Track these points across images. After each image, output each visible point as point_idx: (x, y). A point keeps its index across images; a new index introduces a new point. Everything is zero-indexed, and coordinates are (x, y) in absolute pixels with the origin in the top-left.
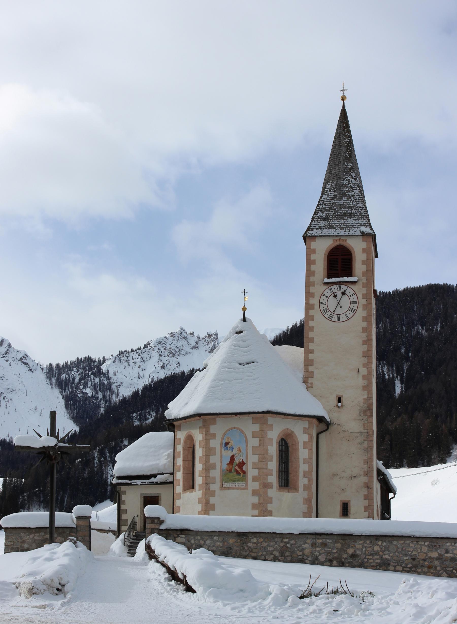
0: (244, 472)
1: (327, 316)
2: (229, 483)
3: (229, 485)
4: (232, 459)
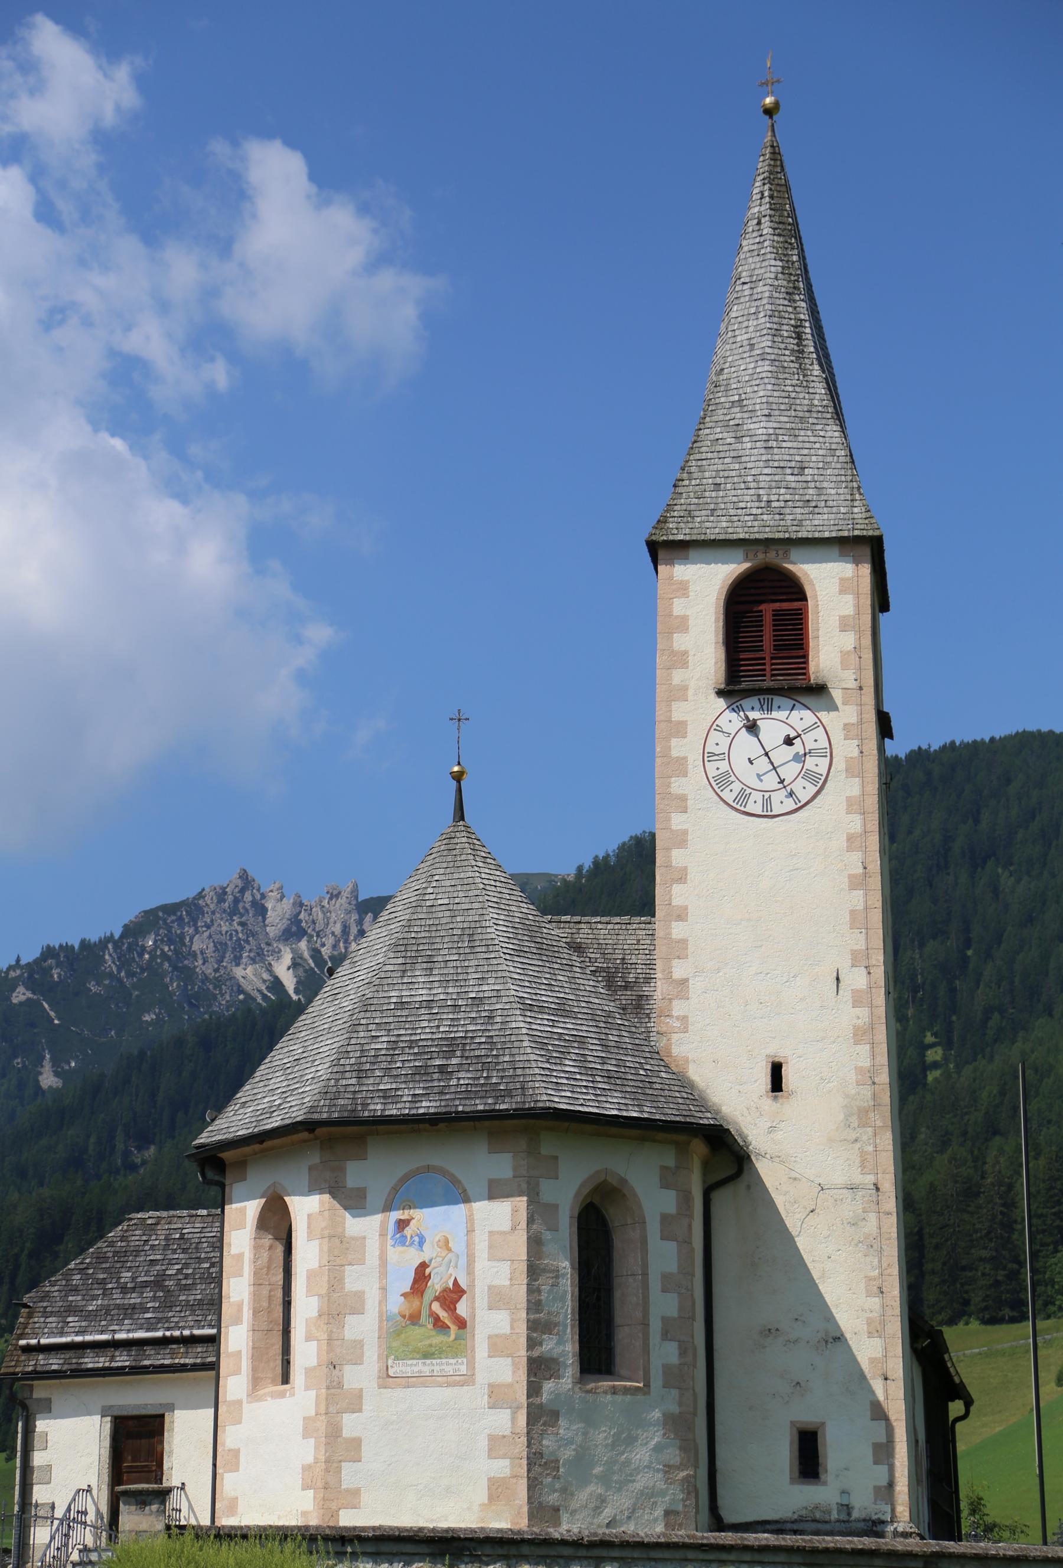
0: (462, 1324)
2: (410, 1362)
3: (409, 1369)
4: (421, 1275)
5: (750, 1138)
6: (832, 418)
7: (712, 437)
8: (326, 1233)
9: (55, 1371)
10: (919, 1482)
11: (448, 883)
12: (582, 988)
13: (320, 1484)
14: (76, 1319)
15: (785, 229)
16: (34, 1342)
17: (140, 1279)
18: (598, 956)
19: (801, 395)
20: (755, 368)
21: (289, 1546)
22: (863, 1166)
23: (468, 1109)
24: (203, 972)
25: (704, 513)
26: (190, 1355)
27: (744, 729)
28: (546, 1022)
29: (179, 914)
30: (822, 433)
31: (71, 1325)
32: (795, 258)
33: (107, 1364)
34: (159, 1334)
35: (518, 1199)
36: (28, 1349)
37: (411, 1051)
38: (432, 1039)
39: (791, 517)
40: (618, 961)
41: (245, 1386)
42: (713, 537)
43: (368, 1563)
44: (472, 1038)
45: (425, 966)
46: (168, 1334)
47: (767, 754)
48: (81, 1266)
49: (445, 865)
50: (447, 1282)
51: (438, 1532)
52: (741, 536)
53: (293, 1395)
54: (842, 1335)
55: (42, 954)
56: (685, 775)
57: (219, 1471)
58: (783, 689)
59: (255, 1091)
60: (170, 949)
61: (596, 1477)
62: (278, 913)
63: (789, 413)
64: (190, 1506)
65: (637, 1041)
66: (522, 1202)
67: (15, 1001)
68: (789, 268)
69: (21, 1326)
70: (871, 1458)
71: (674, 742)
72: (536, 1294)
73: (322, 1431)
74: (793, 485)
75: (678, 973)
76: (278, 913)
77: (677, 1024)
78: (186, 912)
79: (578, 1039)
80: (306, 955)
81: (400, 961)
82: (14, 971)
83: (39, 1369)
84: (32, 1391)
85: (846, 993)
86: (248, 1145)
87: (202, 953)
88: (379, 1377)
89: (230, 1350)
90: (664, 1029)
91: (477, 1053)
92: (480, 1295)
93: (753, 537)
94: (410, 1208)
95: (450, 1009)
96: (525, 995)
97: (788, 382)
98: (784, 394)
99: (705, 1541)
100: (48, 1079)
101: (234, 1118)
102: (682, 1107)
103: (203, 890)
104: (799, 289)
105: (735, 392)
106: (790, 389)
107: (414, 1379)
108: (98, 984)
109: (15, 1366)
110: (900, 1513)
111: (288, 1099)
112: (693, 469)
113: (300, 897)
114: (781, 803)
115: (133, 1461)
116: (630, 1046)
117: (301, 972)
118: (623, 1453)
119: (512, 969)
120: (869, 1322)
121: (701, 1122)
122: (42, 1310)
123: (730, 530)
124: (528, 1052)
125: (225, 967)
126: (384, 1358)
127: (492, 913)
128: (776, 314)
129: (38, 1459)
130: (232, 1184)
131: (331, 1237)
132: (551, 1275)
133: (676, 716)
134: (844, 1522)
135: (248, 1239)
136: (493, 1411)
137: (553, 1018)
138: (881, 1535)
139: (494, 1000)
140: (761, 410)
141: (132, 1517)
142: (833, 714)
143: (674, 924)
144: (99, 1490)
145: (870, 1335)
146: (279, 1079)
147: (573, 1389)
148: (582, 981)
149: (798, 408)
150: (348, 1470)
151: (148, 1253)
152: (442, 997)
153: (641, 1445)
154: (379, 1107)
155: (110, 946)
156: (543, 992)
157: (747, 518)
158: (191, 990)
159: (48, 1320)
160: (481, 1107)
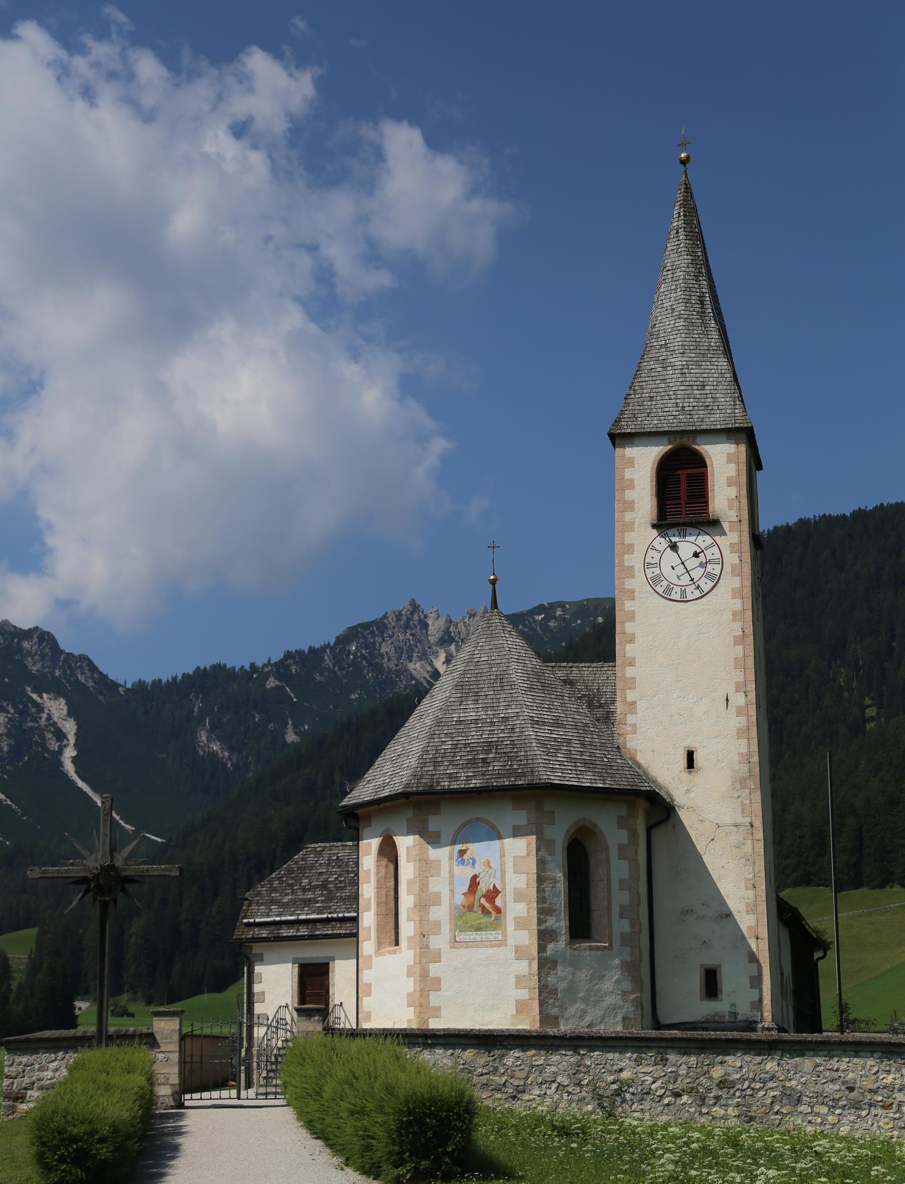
0: (498, 911)
1: (660, 589)
2: (468, 933)
3: (468, 937)
4: (474, 883)
5: (674, 797)
7: (648, 367)
8: (417, 858)
9: (264, 938)
10: (784, 997)
11: (487, 648)
12: (569, 709)
13: (417, 1004)
14: (276, 907)
15: (693, 236)
16: (252, 920)
17: (313, 884)
18: (583, 687)
19: (703, 340)
20: (675, 323)
21: (389, 1040)
22: (743, 812)
23: (499, 784)
24: (388, 666)
25: (643, 415)
26: (343, 929)
28: (547, 731)
29: (371, 629)
30: (716, 363)
32: (700, 254)
33: (294, 934)
34: (325, 916)
35: (531, 837)
36: (248, 925)
38: (478, 743)
39: (697, 416)
40: (595, 691)
41: (374, 947)
42: (648, 430)
43: (441, 1049)
44: (502, 741)
46: (330, 916)
47: (683, 563)
48: (279, 876)
49: (486, 636)
50: (489, 886)
51: (482, 1031)
52: (666, 429)
53: (400, 952)
54: (731, 913)
55: (284, 656)
57: (360, 996)
59: (375, 774)
60: (366, 652)
61: (581, 999)
62: (435, 627)
63: (695, 352)
64: (346, 1015)
65: (603, 741)
67: (268, 687)
69: (244, 911)
71: (626, 557)
72: (542, 893)
73: (418, 973)
74: (698, 396)
75: (630, 698)
76: (435, 627)
78: (377, 627)
81: (459, 695)
82: (267, 668)
85: (732, 709)
86: (372, 806)
87: (387, 654)
88: (450, 942)
89: (364, 926)
90: (622, 732)
91: (505, 750)
93: (673, 429)
95: (489, 724)
96: (534, 715)
98: (692, 340)
99: (638, 1036)
100: (291, 737)
101: (363, 790)
102: (630, 780)
103: (387, 613)
104: (702, 273)
105: (663, 339)
106: (697, 336)
108: (321, 675)
109: (241, 935)
111: (393, 779)
112: (637, 388)
113: (449, 616)
114: (694, 594)
115: (312, 990)
116: (598, 744)
118: (596, 985)
119: (526, 699)
120: (747, 905)
122: (256, 902)
123: (659, 426)
124: (536, 749)
125: (402, 663)
127: (514, 666)
128: (688, 289)
129: (257, 988)
130: (363, 829)
131: (420, 860)
133: (627, 541)
134: (732, 1022)
135: (373, 860)
136: (518, 961)
138: (754, 1030)
139: (515, 718)
141: (303, 1023)
142: (723, 537)
143: (627, 668)
145: (748, 912)
146: (389, 767)
147: (565, 947)
148: (569, 705)
149: (702, 348)
150: (433, 996)
151: (318, 868)
152: (484, 717)
155: (328, 651)
156: (545, 713)
157: (669, 418)
158: (381, 678)
159: (260, 908)
160: (507, 783)
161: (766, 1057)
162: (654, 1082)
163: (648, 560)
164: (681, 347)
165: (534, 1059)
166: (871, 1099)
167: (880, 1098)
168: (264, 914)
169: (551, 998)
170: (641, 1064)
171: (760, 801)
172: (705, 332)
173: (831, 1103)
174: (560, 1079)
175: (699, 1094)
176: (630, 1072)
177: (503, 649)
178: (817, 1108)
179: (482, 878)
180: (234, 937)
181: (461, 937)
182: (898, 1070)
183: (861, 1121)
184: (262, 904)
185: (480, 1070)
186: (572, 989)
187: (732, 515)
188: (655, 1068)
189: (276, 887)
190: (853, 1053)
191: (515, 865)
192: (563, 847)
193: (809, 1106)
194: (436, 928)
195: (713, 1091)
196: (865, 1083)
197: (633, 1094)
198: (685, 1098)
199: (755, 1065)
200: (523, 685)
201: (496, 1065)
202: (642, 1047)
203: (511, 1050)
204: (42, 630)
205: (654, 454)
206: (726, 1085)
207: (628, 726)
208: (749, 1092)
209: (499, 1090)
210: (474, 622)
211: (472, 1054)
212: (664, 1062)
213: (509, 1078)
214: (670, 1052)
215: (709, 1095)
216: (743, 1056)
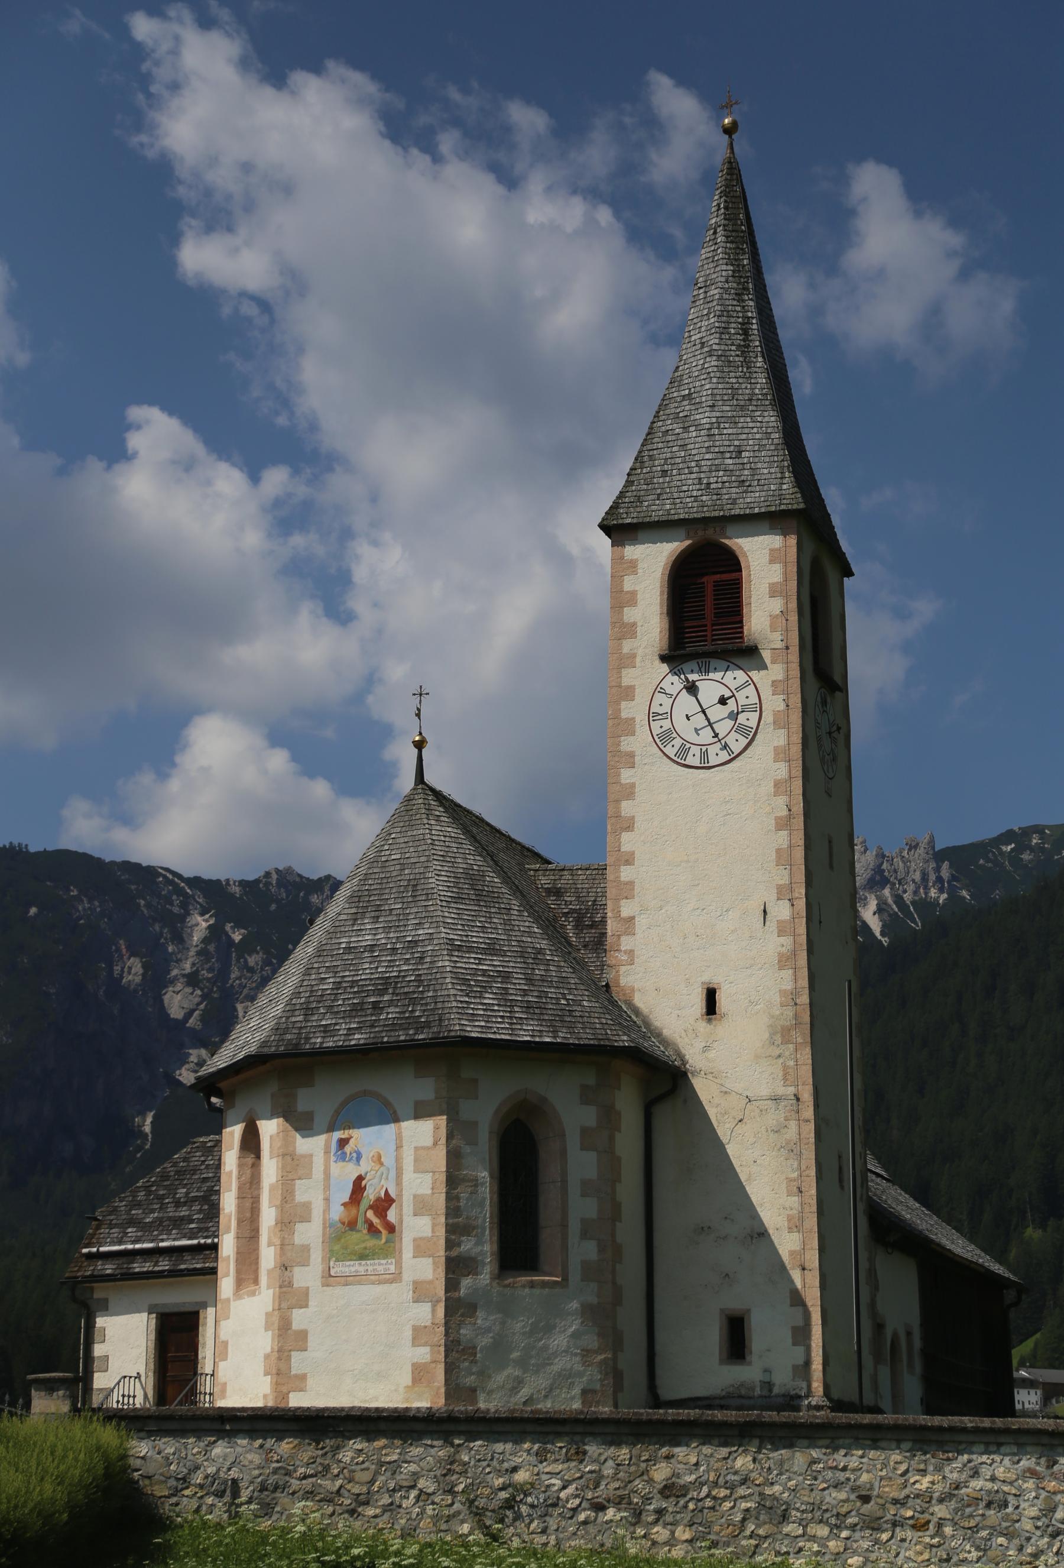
0: (391, 1228)
1: (671, 751)
2: (348, 1263)
3: (347, 1269)
4: (359, 1187)
5: (687, 1057)
6: (771, 404)
9: (108, 1275)
13: (274, 1371)
14: (135, 1229)
17: (192, 1194)
19: (743, 386)
20: (704, 364)
22: (785, 1079)
23: (392, 1039)
25: (651, 497)
27: (684, 690)
28: (472, 961)
30: (759, 419)
31: (130, 1235)
33: (151, 1269)
34: (195, 1242)
35: (439, 1118)
36: (90, 1256)
37: (352, 990)
38: (371, 979)
39: (727, 497)
43: (245, 1439)
44: (404, 976)
45: (373, 914)
46: (202, 1241)
47: (704, 712)
48: (147, 1184)
49: (402, 824)
53: (260, 1293)
54: (766, 1231)
56: (633, 734)
58: (717, 652)
65: (564, 975)
66: (442, 1120)
68: (739, 271)
70: (790, 1341)
71: (623, 704)
73: (276, 1326)
74: (731, 467)
75: (625, 913)
77: (625, 957)
79: (502, 974)
80: (890, 901)
81: (354, 910)
83: (96, 1273)
84: (92, 1293)
85: (772, 925)
88: (323, 1277)
90: (614, 962)
91: (406, 990)
92: (407, 1204)
94: (350, 1129)
96: (456, 937)
97: (732, 374)
98: (728, 386)
104: (748, 289)
105: (686, 386)
106: (734, 380)
107: (351, 1278)
109: (78, 1271)
110: (816, 1388)
114: (716, 755)
116: (556, 979)
117: (885, 916)
118: (541, 1340)
119: (446, 914)
120: (790, 1219)
121: (616, 1044)
123: (672, 512)
126: (326, 1260)
127: (436, 865)
129: (98, 1350)
131: (284, 1155)
132: (470, 1184)
134: (765, 1397)
137: (480, 956)
139: (427, 942)
140: (706, 399)
141: (41, 1401)
142: (763, 673)
143: (623, 868)
144: (146, 1377)
145: (790, 1230)
147: (491, 1283)
148: (517, 923)
149: (740, 397)
152: (383, 941)
153: (559, 1332)
154: (319, 1040)
156: (474, 934)
157: (688, 500)
160: (402, 1038)
161: (736, 1448)
162: (564, 1488)
163: (655, 708)
164: (710, 398)
165: (383, 1452)
166: (895, 1515)
167: (909, 1513)
168: (115, 1240)
169: (465, 1359)
170: (546, 1460)
171: (810, 1061)
172: (748, 375)
173: (833, 1521)
174: (422, 1483)
175: (632, 1506)
176: (528, 1473)
177: (422, 842)
178: (812, 1528)
179: (369, 1181)
180: (67, 1275)
181: (338, 1269)
182: (939, 1469)
183: (879, 1548)
184: (116, 1226)
185: (302, 1470)
186: (500, 1347)
187: (776, 640)
188: (566, 1466)
189: (140, 1201)
190: (869, 1442)
191: (416, 1160)
192: (490, 1133)
193: (800, 1525)
194: (303, 1256)
195: (654, 1501)
196: (887, 1489)
197: (532, 1506)
198: (610, 1513)
199: (719, 1460)
200: (445, 893)
201: (327, 1462)
202: (547, 1433)
203: (350, 1439)
204: (335, 878)
205: (666, 554)
206: (674, 1492)
207: (622, 953)
208: (708, 1503)
209: (330, 1501)
210: (916, 855)
211: (291, 1446)
212: (581, 1456)
213: (346, 1481)
214: (589, 1441)
215: (648, 1507)
216: (700, 1447)
